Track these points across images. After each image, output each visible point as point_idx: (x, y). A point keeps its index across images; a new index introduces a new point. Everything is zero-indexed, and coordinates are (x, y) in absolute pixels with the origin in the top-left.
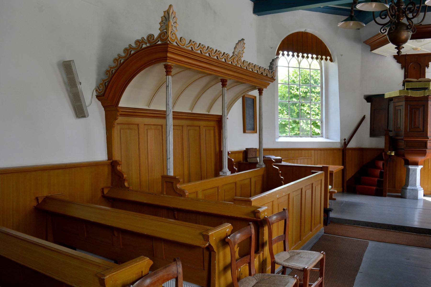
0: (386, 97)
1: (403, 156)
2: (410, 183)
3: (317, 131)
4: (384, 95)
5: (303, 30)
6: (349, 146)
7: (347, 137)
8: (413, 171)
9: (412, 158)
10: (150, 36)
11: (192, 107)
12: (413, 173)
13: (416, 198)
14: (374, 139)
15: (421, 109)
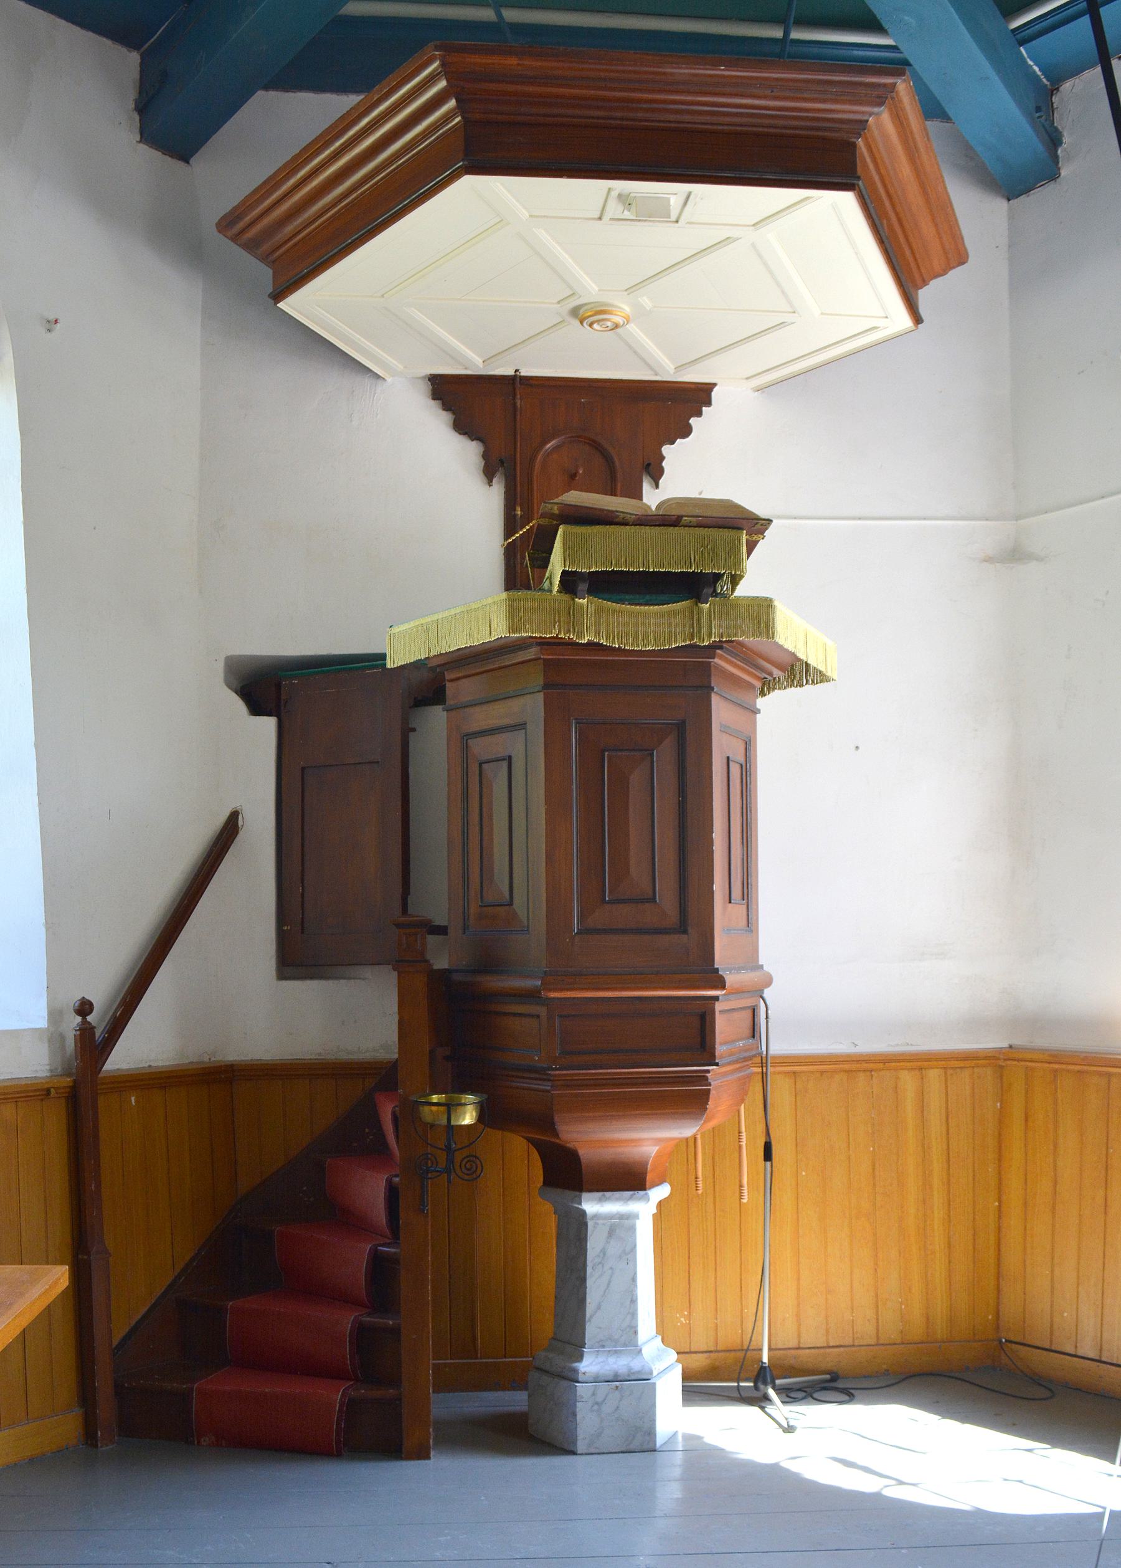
1: (538, 1124)
2: (591, 1331)
4: (382, 657)
7: (101, 987)
8: (611, 1232)
12: (614, 1248)
13: (640, 1442)
14: (307, 992)
15: (664, 755)
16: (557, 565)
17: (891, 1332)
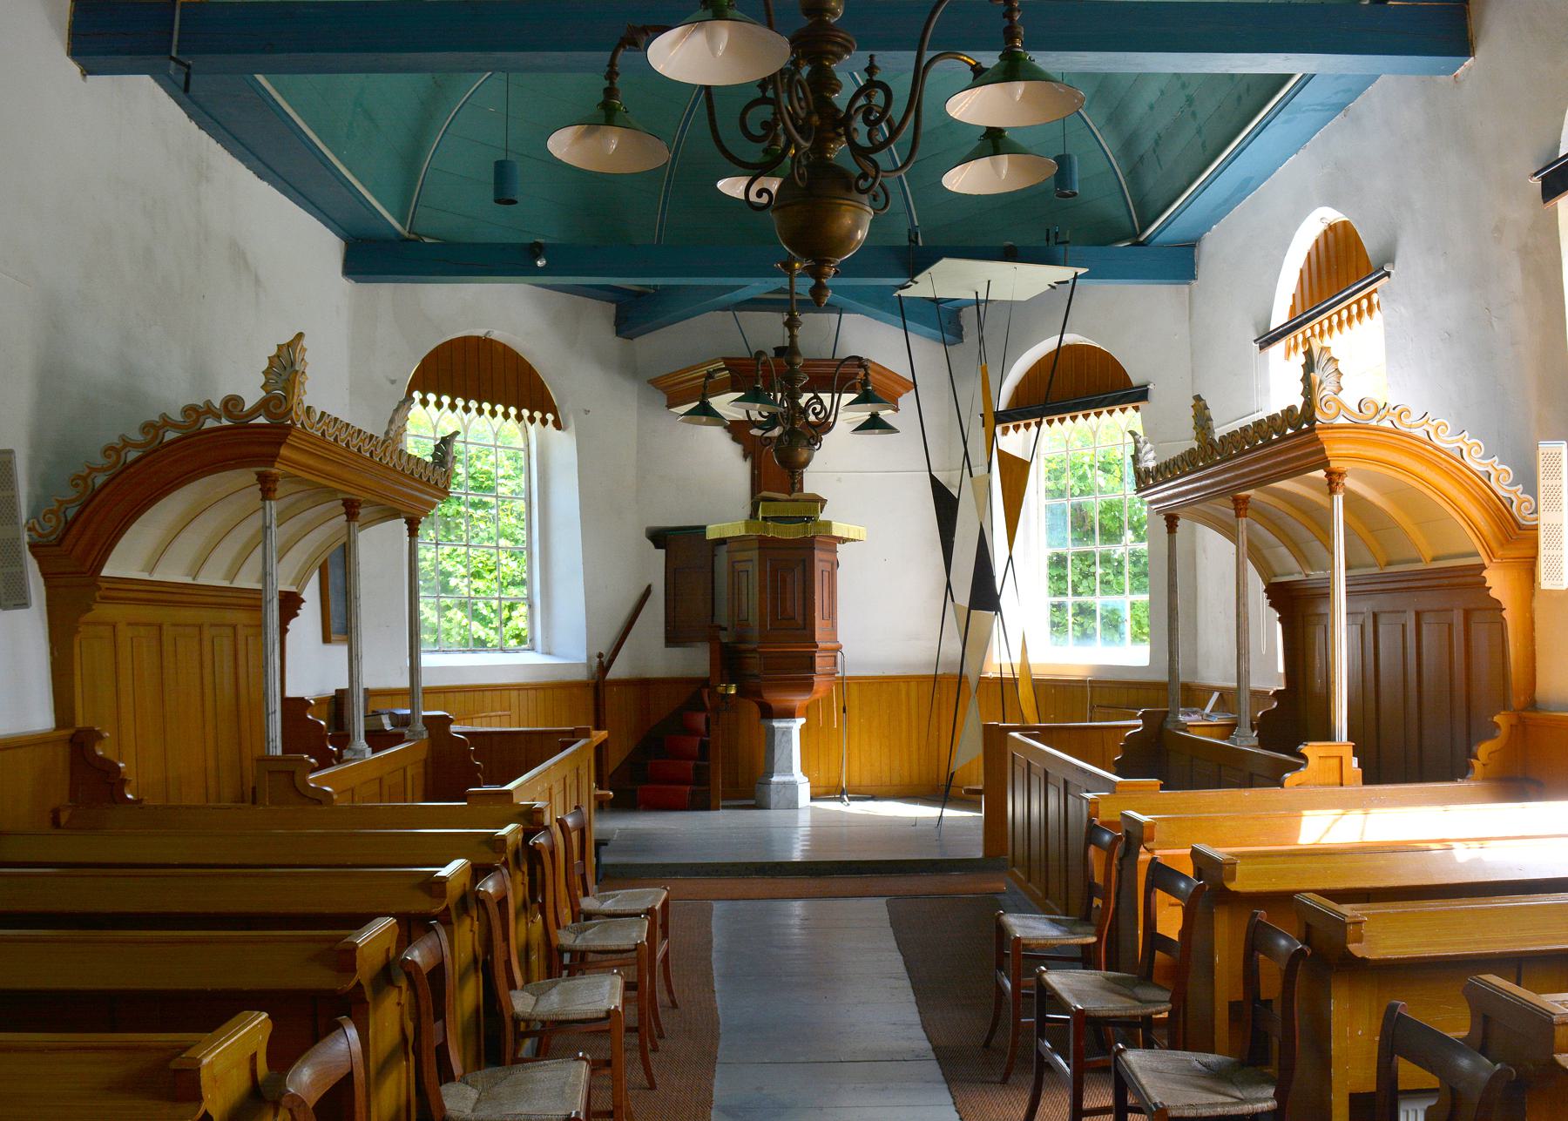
0: (711, 534)
3: (478, 630)
5: (480, 332)
6: (611, 675)
7: (605, 647)
9: (778, 699)
10: (233, 402)
11: (196, 570)
13: (793, 805)
14: (677, 652)
16: (761, 515)
17: (896, 781)
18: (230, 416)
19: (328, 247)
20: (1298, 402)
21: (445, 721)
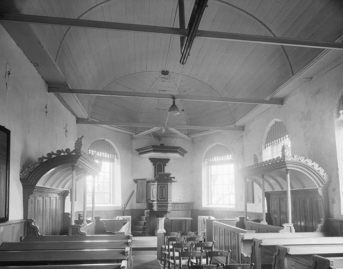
6: (126, 209)
10: (68, 150)
18: (67, 152)
19: (74, 119)
20: (281, 156)
21: (99, 218)
